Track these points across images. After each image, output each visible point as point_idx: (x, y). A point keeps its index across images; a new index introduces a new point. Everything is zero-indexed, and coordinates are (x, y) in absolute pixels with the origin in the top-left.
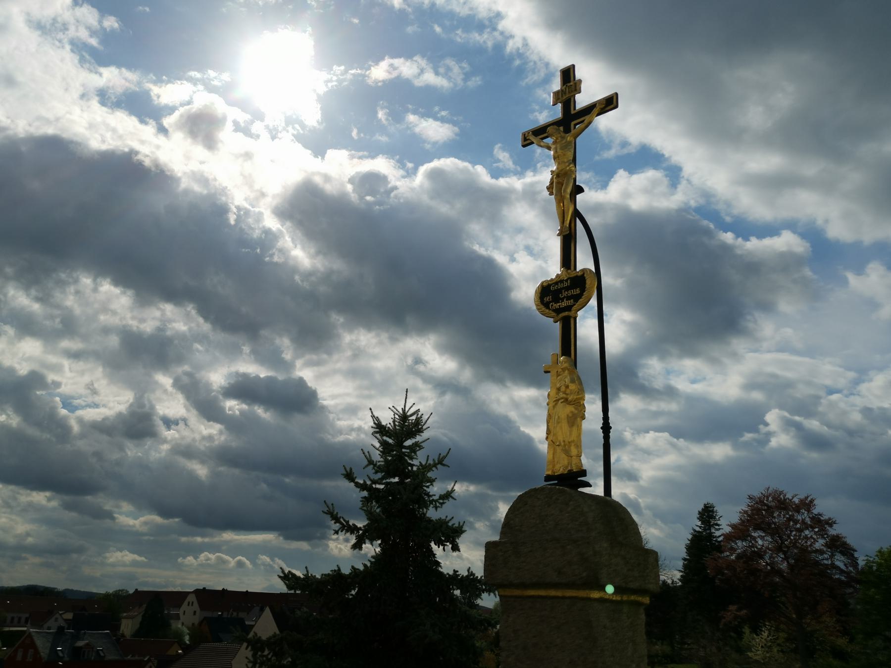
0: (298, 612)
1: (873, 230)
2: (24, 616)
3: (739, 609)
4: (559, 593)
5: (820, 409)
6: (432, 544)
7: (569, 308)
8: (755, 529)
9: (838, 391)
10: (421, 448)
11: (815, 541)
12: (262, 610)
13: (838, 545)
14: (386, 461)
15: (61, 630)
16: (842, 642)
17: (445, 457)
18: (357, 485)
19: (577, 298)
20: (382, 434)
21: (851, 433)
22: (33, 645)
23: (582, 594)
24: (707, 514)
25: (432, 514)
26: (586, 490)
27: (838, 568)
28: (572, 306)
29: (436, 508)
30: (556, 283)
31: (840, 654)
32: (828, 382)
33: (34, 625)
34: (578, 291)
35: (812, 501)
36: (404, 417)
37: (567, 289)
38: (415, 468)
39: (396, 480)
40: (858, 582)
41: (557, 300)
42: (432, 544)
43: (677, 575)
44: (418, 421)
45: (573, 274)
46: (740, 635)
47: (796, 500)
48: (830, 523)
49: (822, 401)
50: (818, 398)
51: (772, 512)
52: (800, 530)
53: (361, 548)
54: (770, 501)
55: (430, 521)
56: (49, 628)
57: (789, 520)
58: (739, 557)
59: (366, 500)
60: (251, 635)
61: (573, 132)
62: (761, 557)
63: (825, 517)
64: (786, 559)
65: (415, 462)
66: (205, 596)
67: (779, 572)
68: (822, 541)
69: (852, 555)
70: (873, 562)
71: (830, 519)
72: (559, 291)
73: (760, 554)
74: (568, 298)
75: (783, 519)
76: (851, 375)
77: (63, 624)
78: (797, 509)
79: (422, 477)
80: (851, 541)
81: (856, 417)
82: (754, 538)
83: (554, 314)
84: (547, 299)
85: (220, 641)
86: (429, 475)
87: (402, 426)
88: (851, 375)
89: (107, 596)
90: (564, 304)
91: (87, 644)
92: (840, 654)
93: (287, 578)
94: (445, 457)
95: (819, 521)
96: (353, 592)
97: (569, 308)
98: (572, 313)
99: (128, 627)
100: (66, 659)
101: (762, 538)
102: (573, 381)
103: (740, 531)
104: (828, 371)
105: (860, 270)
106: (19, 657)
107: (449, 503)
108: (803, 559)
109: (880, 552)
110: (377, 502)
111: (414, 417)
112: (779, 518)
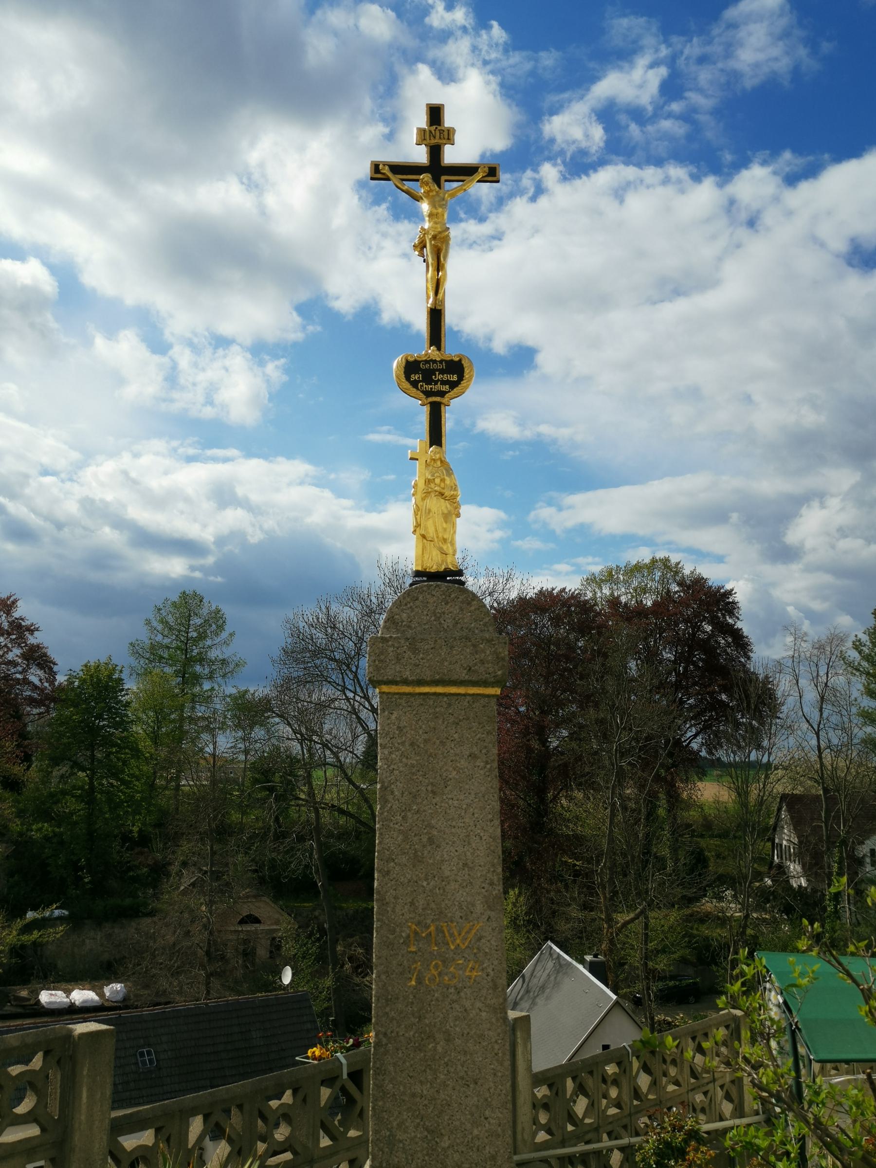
1: (138, 289)
4: (461, 690)
5: (27, 491)
9: (54, 473)
11: (9, 650)
13: (37, 657)
19: (453, 385)
21: (59, 526)
28: (447, 392)
30: (426, 362)
32: (45, 460)
34: (455, 378)
35: (14, 602)
37: (442, 372)
40: (54, 700)
48: (32, 630)
49: (31, 481)
50: (26, 476)
63: (28, 623)
68: (17, 651)
69: (51, 669)
70: (75, 677)
71: (32, 625)
72: (433, 372)
74: (444, 383)
76: (75, 455)
80: (53, 654)
81: (71, 508)
83: (422, 395)
84: (414, 377)
88: (75, 455)
90: (439, 387)
95: (20, 626)
97: (442, 394)
98: (445, 400)
104: (50, 446)
105: (111, 334)
109: (86, 666)
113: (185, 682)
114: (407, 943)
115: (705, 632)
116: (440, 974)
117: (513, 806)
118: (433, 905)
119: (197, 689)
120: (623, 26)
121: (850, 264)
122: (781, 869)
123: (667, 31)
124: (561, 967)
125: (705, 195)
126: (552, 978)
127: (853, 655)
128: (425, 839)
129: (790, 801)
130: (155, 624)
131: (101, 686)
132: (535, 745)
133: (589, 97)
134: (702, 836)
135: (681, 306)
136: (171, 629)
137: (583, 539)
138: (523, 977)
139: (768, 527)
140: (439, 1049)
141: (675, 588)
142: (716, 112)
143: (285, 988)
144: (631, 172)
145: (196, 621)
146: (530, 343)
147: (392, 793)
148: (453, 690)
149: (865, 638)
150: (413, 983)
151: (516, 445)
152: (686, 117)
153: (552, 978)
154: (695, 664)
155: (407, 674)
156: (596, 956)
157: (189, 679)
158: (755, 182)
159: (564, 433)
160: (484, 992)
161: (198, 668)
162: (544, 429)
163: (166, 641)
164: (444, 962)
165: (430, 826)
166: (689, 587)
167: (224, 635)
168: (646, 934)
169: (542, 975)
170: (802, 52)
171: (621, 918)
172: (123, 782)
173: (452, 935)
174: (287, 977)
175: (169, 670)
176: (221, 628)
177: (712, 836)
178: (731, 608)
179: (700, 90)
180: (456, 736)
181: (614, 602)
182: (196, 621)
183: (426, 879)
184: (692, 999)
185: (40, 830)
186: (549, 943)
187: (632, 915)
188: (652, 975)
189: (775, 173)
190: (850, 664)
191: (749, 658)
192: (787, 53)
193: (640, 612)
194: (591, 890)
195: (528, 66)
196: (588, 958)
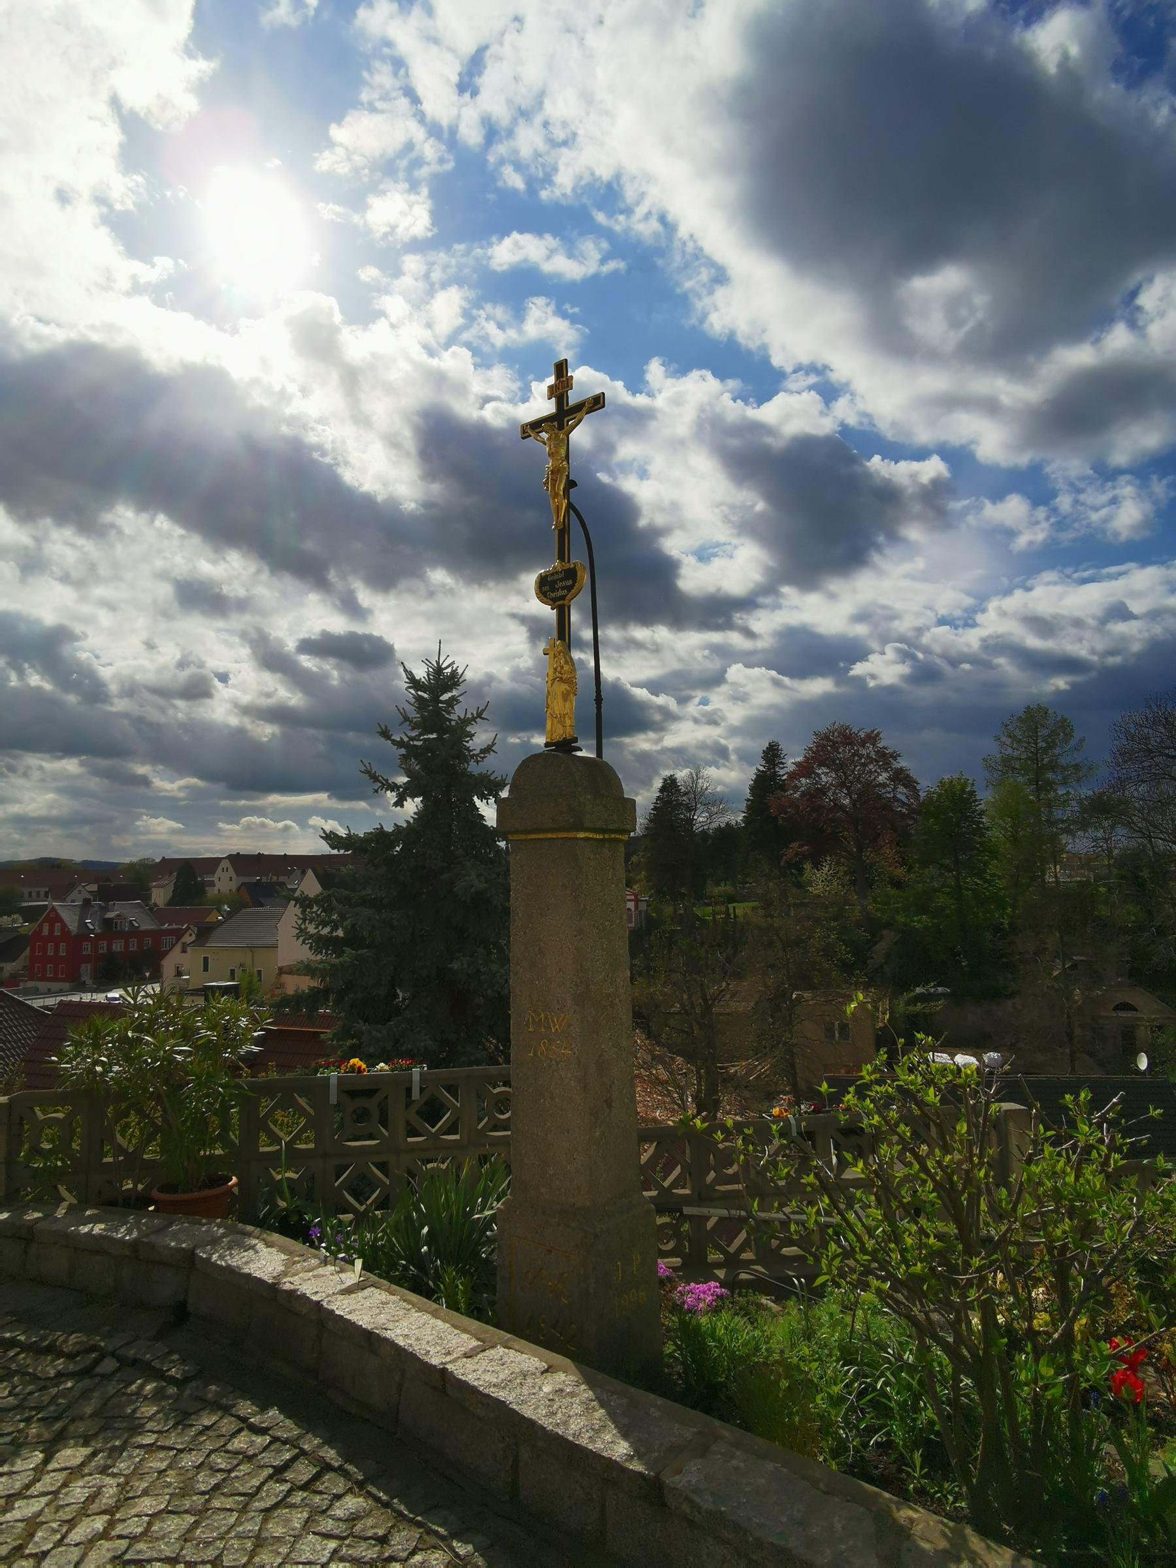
0: (343, 869)
2: (43, 890)
3: (801, 846)
6: (475, 798)
7: (563, 598)
8: (820, 766)
10: (458, 702)
11: (879, 774)
12: (304, 873)
13: (901, 777)
14: (422, 717)
15: (87, 902)
16: (900, 872)
17: (483, 711)
18: (394, 742)
19: (569, 588)
20: (417, 690)
22: (58, 919)
23: (571, 835)
24: (772, 754)
25: (473, 768)
26: (579, 754)
27: (899, 800)
29: (478, 762)
30: (552, 574)
31: (898, 884)
33: (55, 899)
36: (439, 670)
37: (561, 580)
38: (453, 723)
39: (434, 736)
40: (919, 813)
41: (553, 590)
42: (475, 798)
43: (740, 817)
44: (454, 673)
45: (567, 566)
46: (801, 871)
47: (862, 734)
51: (838, 746)
52: (864, 765)
53: (402, 806)
54: (835, 737)
55: (471, 776)
56: (73, 901)
57: (854, 755)
58: (803, 794)
59: (405, 758)
60: (297, 894)
61: (566, 428)
62: (825, 794)
63: (891, 751)
64: (849, 794)
65: (452, 717)
66: (239, 861)
67: (842, 808)
68: (885, 775)
72: (555, 582)
73: (822, 791)
74: (563, 588)
75: (848, 755)
77: (88, 896)
78: (863, 744)
79: (461, 731)
82: (818, 775)
84: (546, 588)
85: (262, 905)
86: (468, 729)
87: (437, 679)
89: (132, 866)
90: (560, 593)
91: (118, 915)
92: (898, 884)
93: (330, 837)
94: (483, 711)
95: (884, 754)
96: (398, 849)
97: (563, 598)
99: (160, 896)
100: (98, 931)
101: (826, 774)
102: (566, 662)
103: (805, 769)
106: (46, 932)
107: (491, 757)
108: (868, 794)
110: (416, 759)
111: (449, 670)
112: (844, 753)
113: (1038, 790)
119: (1052, 794)
130: (1004, 739)
131: (956, 801)
136: (1019, 741)
143: (1138, 1072)
145: (1043, 732)
157: (1041, 785)
161: (1050, 775)
163: (1016, 753)
167: (1073, 742)
172: (986, 881)
174: (1143, 1063)
175: (1021, 779)
176: (1068, 735)
182: (1043, 732)
185: (921, 921)
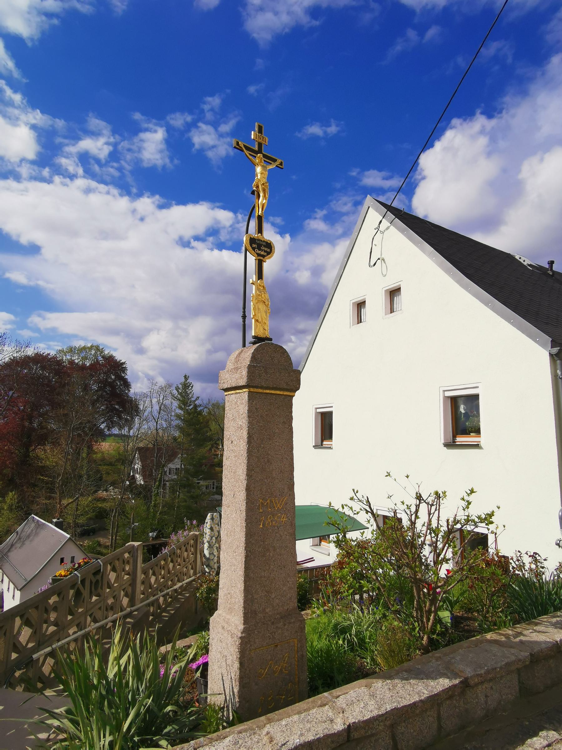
4: (281, 393)
114: (258, 509)
115: (111, 378)
116: (271, 521)
117: (12, 453)
118: (269, 490)
120: (94, 122)
121: (177, 244)
122: (134, 477)
123: (114, 132)
124: (39, 526)
125: (124, 203)
126: (34, 531)
127: (175, 392)
128: (266, 460)
129: (140, 449)
132: (27, 424)
133: (77, 146)
134: (100, 465)
135: (106, 245)
137: (52, 334)
138: (17, 532)
139: (135, 338)
140: (271, 555)
141: (100, 358)
142: (132, 172)
144: (94, 184)
146: (39, 243)
147: (253, 439)
148: (278, 392)
149: (180, 386)
150: (261, 526)
151: (24, 287)
152: (120, 169)
153: (34, 531)
154: (106, 392)
155: (263, 384)
156: (58, 519)
158: (146, 204)
159: (51, 286)
160: (288, 527)
162: (41, 283)
164: (273, 515)
165: (268, 454)
166: (107, 359)
168: (77, 508)
169: (28, 530)
170: (167, 161)
171: (65, 502)
173: (276, 503)
177: (104, 465)
178: (124, 370)
179: (126, 161)
180: (278, 413)
181: (72, 362)
183: (266, 479)
184: (91, 534)
186: (33, 515)
187: (71, 500)
188: (77, 525)
189: (153, 203)
190: (173, 395)
191: (129, 391)
192: (161, 159)
193: (83, 368)
194: (52, 491)
195: (50, 122)
196: (55, 520)
